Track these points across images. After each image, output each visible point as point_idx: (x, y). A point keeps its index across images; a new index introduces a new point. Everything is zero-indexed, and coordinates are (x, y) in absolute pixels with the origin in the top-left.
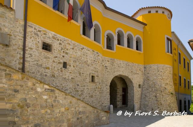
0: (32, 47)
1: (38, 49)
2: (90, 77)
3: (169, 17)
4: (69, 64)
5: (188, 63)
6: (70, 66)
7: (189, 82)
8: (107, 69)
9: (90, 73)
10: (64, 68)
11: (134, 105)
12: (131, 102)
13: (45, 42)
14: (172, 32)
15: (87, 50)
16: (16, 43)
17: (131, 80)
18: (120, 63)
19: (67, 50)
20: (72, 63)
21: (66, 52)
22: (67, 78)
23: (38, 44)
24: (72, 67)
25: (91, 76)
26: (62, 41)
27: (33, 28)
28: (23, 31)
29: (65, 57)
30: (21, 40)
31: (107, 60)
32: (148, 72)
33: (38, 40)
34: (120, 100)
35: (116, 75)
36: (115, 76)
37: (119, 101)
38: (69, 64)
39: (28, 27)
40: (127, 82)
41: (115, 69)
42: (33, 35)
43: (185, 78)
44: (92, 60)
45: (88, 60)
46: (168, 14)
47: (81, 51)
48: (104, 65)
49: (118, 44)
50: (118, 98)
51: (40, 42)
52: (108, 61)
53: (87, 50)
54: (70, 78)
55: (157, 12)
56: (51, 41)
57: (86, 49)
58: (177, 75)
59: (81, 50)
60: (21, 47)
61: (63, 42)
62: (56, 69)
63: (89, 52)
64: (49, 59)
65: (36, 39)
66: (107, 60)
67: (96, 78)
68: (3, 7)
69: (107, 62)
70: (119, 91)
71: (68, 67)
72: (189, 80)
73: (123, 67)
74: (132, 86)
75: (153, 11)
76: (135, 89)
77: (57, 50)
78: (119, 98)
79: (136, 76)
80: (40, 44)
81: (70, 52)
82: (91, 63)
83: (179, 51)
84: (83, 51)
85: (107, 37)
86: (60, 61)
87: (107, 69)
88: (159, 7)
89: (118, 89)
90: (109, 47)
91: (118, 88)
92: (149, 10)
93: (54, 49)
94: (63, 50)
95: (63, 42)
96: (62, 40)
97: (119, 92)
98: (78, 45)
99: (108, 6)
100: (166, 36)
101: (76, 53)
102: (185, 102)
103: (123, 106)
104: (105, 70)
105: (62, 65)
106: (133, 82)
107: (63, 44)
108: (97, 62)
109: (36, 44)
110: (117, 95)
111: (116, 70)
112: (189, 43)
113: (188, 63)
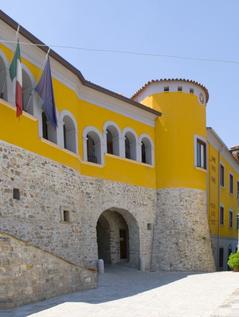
2: (60, 212)
3: (202, 99)
6: (25, 195)
8: (90, 197)
9: (61, 207)
11: (139, 259)
15: (52, 165)
17: (133, 216)
19: (18, 167)
20: (28, 190)
22: (21, 215)
25: (62, 212)
26: (8, 152)
31: (89, 182)
34: (117, 251)
35: (107, 208)
37: (114, 253)
44: (62, 183)
47: (42, 168)
50: (113, 247)
52: (91, 184)
55: (180, 89)
58: (217, 206)
59: (41, 165)
61: (9, 153)
70: (114, 235)
71: (21, 197)
73: (118, 194)
78: (115, 247)
79: (141, 209)
84: (45, 167)
86: (7, 187)
87: (90, 197)
90: (93, 157)
92: (166, 85)
94: (10, 168)
95: (9, 153)
96: (8, 150)
97: (114, 236)
99: (87, 78)
100: (196, 137)
101: (33, 172)
104: (86, 200)
105: (11, 195)
107: (10, 157)
108: (71, 186)
110: (111, 242)
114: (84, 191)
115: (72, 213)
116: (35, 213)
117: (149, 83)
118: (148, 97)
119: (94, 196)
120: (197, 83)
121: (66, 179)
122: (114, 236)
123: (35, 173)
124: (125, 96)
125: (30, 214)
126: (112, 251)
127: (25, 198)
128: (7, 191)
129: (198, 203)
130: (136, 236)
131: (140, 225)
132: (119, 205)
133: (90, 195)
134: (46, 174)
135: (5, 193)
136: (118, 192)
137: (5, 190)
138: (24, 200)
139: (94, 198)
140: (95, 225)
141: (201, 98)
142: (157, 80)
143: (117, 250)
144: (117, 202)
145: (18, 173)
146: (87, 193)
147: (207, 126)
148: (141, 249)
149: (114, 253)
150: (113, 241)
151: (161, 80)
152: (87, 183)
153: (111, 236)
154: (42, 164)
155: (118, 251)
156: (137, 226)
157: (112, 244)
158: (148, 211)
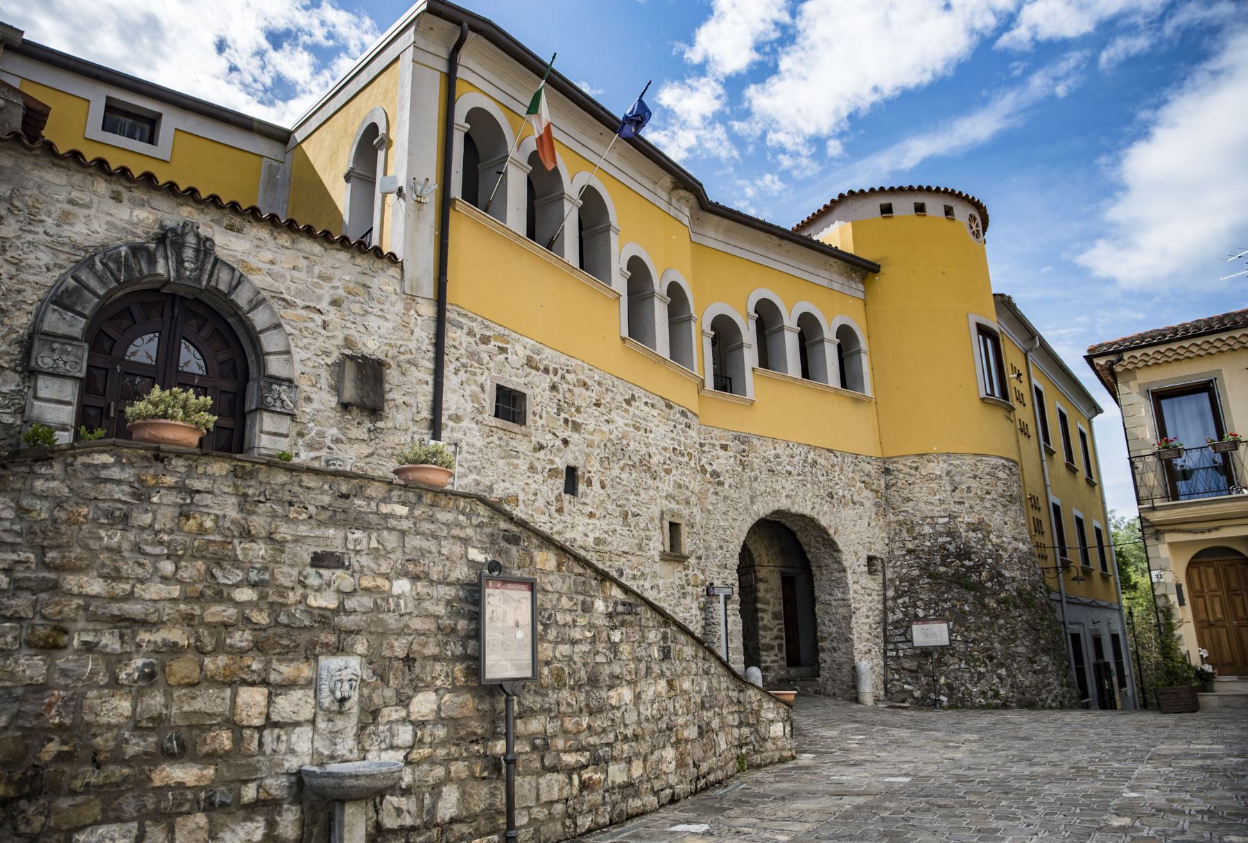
0: (460, 413)
1: (480, 418)
2: (662, 528)
3: (974, 228)
4: (587, 475)
5: (1083, 435)
6: (589, 483)
7: (1098, 532)
8: (720, 484)
9: (662, 513)
10: (568, 497)
11: (854, 668)
12: (835, 649)
13: (501, 383)
14: (994, 295)
15: (646, 403)
16: (406, 399)
17: (829, 535)
18: (777, 456)
19: (578, 410)
20: (594, 466)
21: (574, 423)
22: (578, 538)
23: (482, 396)
24: (596, 485)
25: (666, 525)
26: (559, 375)
27: (465, 330)
28: (431, 348)
29: (571, 446)
30: (425, 386)
31: (717, 443)
32: (906, 493)
33: (481, 379)
34: (775, 643)
35: (762, 515)
36: (756, 519)
37: (769, 648)
38: (587, 475)
39: (448, 326)
40: (806, 548)
41: (755, 485)
42: (464, 360)
43: (1080, 515)
44: (665, 449)
45: (653, 450)
46: (971, 216)
47: (626, 411)
48: (709, 469)
49: (760, 366)
50: (766, 628)
51: (488, 386)
52: (724, 447)
53: (646, 403)
54: (590, 540)
55: (920, 209)
56: (523, 380)
57: (645, 400)
58: (1042, 504)
59: (624, 405)
60: (426, 414)
61: (563, 377)
62: (541, 503)
63: (655, 412)
64: (515, 461)
65: (475, 374)
66: (717, 443)
67: (684, 530)
68: (365, 256)
69: (721, 453)
70: (766, 591)
71: (582, 487)
72: (1099, 526)
73: (790, 473)
74: (836, 566)
75: (904, 206)
76: (850, 581)
77: (544, 414)
78: (771, 629)
79: (849, 513)
80: (486, 396)
81: (589, 419)
82: (665, 463)
83: (1034, 381)
84: (631, 409)
85: (713, 333)
87: (720, 484)
88: (929, 189)
89: (761, 580)
90: (726, 380)
91: (760, 575)
92: (884, 200)
93: (535, 414)
95: (563, 377)
96: (560, 372)
97: (769, 596)
98: (613, 386)
99: (713, 195)
100: (974, 319)
101: (608, 422)
102: (1097, 641)
103: (793, 671)
104: (712, 490)
105: (560, 482)
106: (841, 546)
107: (563, 387)
108: (683, 455)
109: (474, 398)
110: (760, 615)
111: (763, 488)
112: (1089, 359)
113: (1083, 435)
114: (707, 467)
115: (687, 529)
116: (607, 533)
117: (841, 196)
118: (25, 37)
119: (731, 481)
120: (960, 193)
121: (673, 439)
122: (769, 596)
123: (611, 426)
124: (784, 227)
125: (597, 535)
126: (763, 641)
127: (588, 491)
128: (553, 473)
129: (1002, 496)
130: (840, 596)
131: (848, 559)
132: (793, 504)
133: (721, 479)
134: (634, 426)
135: (549, 480)
136: (789, 468)
137: (550, 470)
138: (586, 495)
139: (730, 486)
140: (734, 562)
141: (974, 226)
142: (862, 191)
143: (777, 638)
144: (787, 496)
145: (576, 427)
146: (715, 474)
147: (994, 291)
148: (855, 636)
149: (769, 648)
150: (764, 611)
151: (872, 190)
152: (714, 445)
153: (759, 595)
154: (625, 400)
155: (778, 642)
156: (840, 563)
157: (762, 619)
158: (866, 520)
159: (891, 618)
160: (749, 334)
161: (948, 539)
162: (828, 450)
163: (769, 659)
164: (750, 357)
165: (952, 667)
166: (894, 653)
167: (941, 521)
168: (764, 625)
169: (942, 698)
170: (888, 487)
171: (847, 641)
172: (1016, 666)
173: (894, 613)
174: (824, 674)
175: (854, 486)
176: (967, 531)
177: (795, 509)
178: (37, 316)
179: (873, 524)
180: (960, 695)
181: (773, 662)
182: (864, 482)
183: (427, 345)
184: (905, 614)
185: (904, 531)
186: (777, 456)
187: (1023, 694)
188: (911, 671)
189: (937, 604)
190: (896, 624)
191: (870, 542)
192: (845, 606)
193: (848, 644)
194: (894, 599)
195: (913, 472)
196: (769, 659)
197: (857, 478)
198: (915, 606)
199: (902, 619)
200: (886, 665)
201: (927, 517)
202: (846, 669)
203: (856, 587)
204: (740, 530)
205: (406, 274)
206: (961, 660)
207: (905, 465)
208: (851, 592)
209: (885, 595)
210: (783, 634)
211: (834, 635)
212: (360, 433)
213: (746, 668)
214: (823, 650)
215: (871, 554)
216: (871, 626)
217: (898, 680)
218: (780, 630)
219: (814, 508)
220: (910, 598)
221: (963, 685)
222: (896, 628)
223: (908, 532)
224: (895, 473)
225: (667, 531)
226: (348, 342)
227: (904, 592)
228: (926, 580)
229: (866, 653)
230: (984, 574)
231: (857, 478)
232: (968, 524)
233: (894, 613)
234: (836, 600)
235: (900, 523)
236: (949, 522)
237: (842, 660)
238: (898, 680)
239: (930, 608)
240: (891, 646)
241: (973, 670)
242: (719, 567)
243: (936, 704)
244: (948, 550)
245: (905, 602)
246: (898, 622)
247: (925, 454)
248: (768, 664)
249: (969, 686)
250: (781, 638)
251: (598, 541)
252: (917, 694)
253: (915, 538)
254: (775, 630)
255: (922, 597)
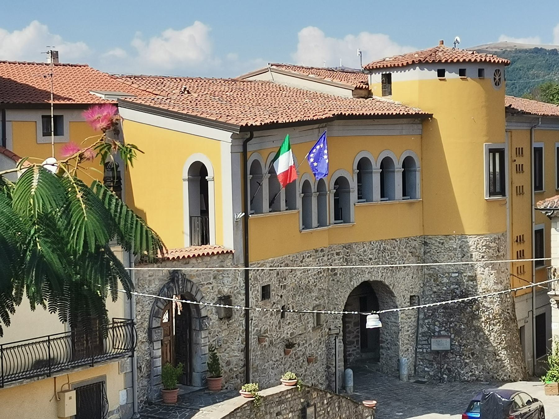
17: (389, 289)
28: (244, 285)
34: (355, 340)
52: (338, 254)
66: (335, 252)
69: (336, 257)
74: (392, 303)
139: (340, 275)
156: (395, 303)
157: (349, 327)
159: (421, 330)
160: (353, 184)
161: (457, 286)
162: (392, 239)
163: (351, 350)
164: (354, 196)
165: (451, 360)
166: (421, 350)
167: (453, 275)
168: (350, 331)
169: (445, 376)
170: (425, 253)
171: (396, 345)
172: (486, 358)
173: (422, 327)
174: (382, 361)
175: (405, 257)
176: (468, 281)
177: (373, 279)
178: (149, 322)
179: (415, 276)
180: (454, 375)
181: (353, 350)
182: (411, 252)
183: (243, 284)
184: (429, 329)
185: (432, 280)
186: (365, 251)
187: (488, 373)
188: (430, 361)
189: (446, 324)
190: (424, 334)
191: (412, 288)
192: (396, 326)
193: (396, 347)
194: (424, 319)
195: (440, 245)
196: (351, 350)
197: (407, 251)
198: (435, 325)
199: (427, 332)
200: (416, 356)
201: (446, 273)
202: (394, 360)
203: (403, 315)
204: (344, 297)
205: (235, 257)
206: (456, 356)
207: (436, 241)
208: (400, 319)
209: (418, 317)
210: (360, 334)
211: (389, 341)
212: (225, 327)
213: (345, 370)
214: (382, 348)
215: (412, 295)
216: (409, 336)
217: (422, 365)
218: (358, 332)
219: (382, 275)
220: (432, 320)
221: (456, 369)
222: (423, 336)
223: (434, 281)
224: (430, 245)
225: (315, 317)
226: (219, 292)
227: (429, 316)
228: (442, 310)
229: (406, 351)
230: (474, 306)
231: (407, 251)
232: (469, 276)
233: (422, 327)
234: (391, 322)
235: (431, 275)
236: (458, 276)
237: (392, 355)
238: (422, 365)
239: (443, 326)
240: (419, 346)
241: (462, 361)
242: (333, 319)
243: (441, 380)
244: (456, 293)
245: (429, 322)
246: (424, 333)
247: (449, 235)
248: (350, 352)
249: (459, 369)
250: (358, 336)
251: (291, 335)
252: (431, 373)
253: (438, 285)
254: (355, 332)
255: (439, 319)
